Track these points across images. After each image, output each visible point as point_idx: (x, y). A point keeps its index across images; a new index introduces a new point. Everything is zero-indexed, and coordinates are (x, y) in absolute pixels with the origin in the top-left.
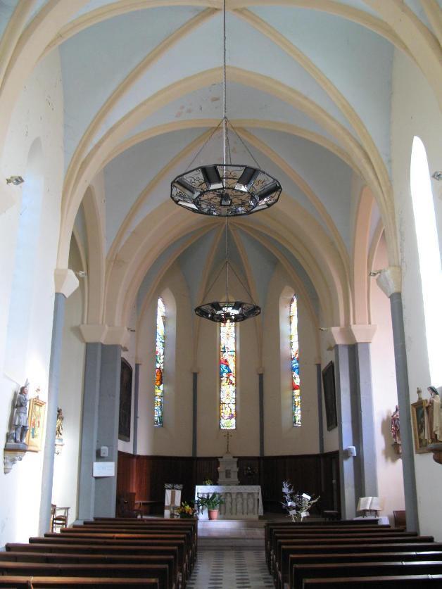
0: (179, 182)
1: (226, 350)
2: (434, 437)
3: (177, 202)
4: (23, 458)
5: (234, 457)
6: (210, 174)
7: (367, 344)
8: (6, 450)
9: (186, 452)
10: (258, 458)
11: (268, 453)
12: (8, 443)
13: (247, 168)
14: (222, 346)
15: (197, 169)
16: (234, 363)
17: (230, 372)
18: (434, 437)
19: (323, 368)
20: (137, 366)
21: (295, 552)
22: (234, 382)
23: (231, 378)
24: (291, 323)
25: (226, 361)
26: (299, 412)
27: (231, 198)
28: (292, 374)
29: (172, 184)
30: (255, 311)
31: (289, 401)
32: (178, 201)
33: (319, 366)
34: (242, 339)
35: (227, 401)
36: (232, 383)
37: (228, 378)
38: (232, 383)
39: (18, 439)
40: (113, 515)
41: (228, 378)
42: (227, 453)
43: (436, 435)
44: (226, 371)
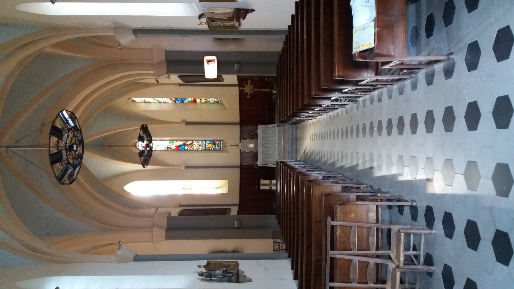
0: (60, 179)
1: (169, 146)
2: (230, 19)
3: (74, 180)
4: (243, 271)
5: (240, 142)
6: (55, 158)
7: (167, 53)
8: (237, 281)
9: (238, 171)
10: (241, 127)
11: (237, 119)
12: (234, 280)
13: (51, 134)
14: (166, 149)
15: (52, 168)
16: (178, 142)
17: (184, 144)
18: (230, 19)
19: (181, 82)
20: (181, 206)
21: (287, 115)
22: (191, 142)
23: (189, 143)
24: (150, 102)
25: (176, 147)
26: (211, 99)
27: (72, 144)
28: (186, 103)
29: (62, 184)
30: (144, 128)
31: (204, 106)
32: (73, 179)
33: (180, 85)
34: (162, 135)
35: (204, 146)
36: (192, 143)
37: (188, 145)
38: (192, 143)
39: (231, 275)
40: (275, 216)
41: (188, 145)
42: (238, 147)
43: (229, 17)
44: (183, 147)
